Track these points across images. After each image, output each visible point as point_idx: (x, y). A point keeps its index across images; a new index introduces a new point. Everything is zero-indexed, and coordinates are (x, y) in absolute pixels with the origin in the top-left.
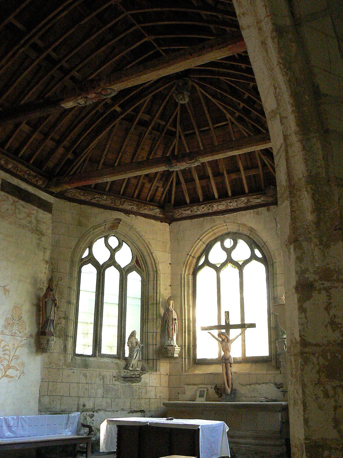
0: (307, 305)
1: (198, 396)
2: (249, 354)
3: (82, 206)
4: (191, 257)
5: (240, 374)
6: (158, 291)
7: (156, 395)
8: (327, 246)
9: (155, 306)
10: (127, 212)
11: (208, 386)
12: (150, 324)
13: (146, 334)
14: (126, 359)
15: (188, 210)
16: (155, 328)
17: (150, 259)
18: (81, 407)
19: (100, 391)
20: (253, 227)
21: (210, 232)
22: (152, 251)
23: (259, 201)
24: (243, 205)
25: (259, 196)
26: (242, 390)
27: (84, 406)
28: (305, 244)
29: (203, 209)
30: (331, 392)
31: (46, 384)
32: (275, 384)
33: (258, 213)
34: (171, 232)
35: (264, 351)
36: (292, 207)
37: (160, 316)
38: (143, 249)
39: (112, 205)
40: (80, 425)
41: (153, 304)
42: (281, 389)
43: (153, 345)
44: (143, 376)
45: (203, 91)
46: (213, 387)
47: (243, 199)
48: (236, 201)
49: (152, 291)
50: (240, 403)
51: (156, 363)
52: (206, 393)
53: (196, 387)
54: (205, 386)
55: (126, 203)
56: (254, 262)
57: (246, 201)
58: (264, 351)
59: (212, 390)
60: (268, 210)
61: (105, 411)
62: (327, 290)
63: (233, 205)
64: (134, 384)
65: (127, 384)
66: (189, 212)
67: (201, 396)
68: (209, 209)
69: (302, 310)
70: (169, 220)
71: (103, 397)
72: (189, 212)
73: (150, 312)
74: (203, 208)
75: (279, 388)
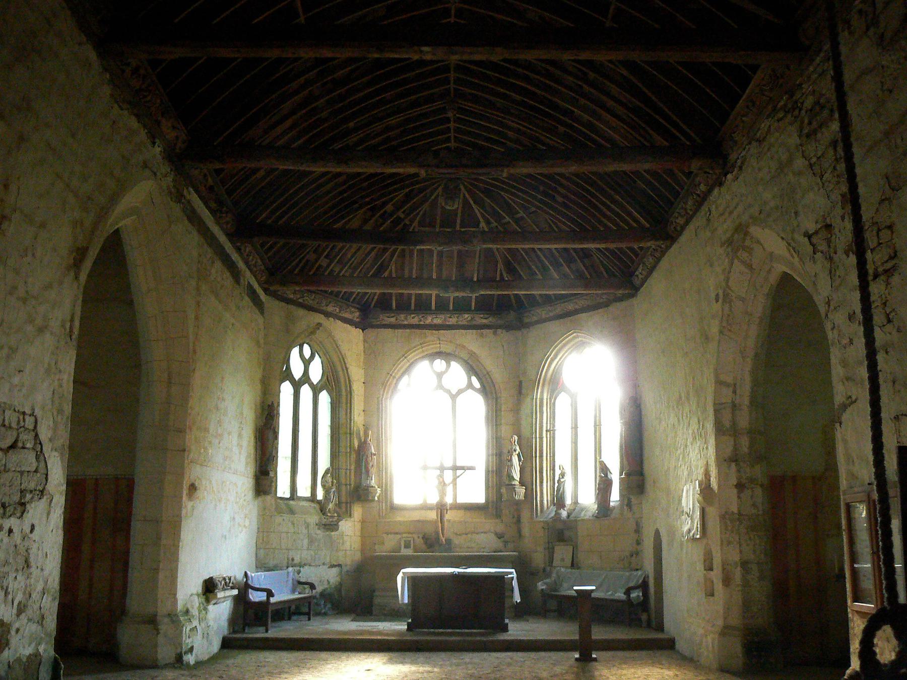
0: (742, 495)
1: (403, 546)
2: (459, 501)
3: (290, 307)
4: (391, 377)
5: (455, 522)
6: (352, 418)
7: (351, 547)
8: (753, 466)
9: (348, 436)
10: (327, 315)
11: (414, 535)
12: (342, 459)
13: (337, 471)
14: (319, 502)
15: (392, 317)
16: (348, 464)
17: (344, 375)
18: (290, 562)
19: (306, 542)
20: (475, 351)
21: (418, 349)
22: (348, 366)
23: (484, 321)
24: (465, 323)
25: (486, 316)
26: (456, 541)
27: (293, 560)
28: (741, 464)
29: (414, 320)
30: (752, 537)
31: (261, 535)
32: (496, 534)
33: (482, 335)
34: (365, 341)
35: (479, 497)
36: (735, 441)
37: (354, 450)
38: (335, 359)
39: (316, 306)
40: (296, 583)
41: (346, 433)
42: (502, 539)
43: (346, 485)
44: (340, 523)
45: (467, 195)
46: (421, 536)
47: (466, 316)
48: (458, 317)
49: (344, 417)
50: (503, 553)
51: (350, 507)
52: (412, 542)
53: (398, 536)
54: (410, 535)
55: (331, 304)
56: (470, 391)
57: (469, 318)
58: (479, 497)
59: (419, 540)
60: (495, 333)
61: (310, 566)
62: (752, 488)
63: (453, 321)
64: (333, 533)
65: (328, 533)
66: (393, 320)
67: (407, 546)
68: (421, 321)
69: (739, 497)
70: (364, 324)
71: (308, 549)
72: (393, 320)
73: (342, 444)
74: (413, 318)
75: (499, 538)
